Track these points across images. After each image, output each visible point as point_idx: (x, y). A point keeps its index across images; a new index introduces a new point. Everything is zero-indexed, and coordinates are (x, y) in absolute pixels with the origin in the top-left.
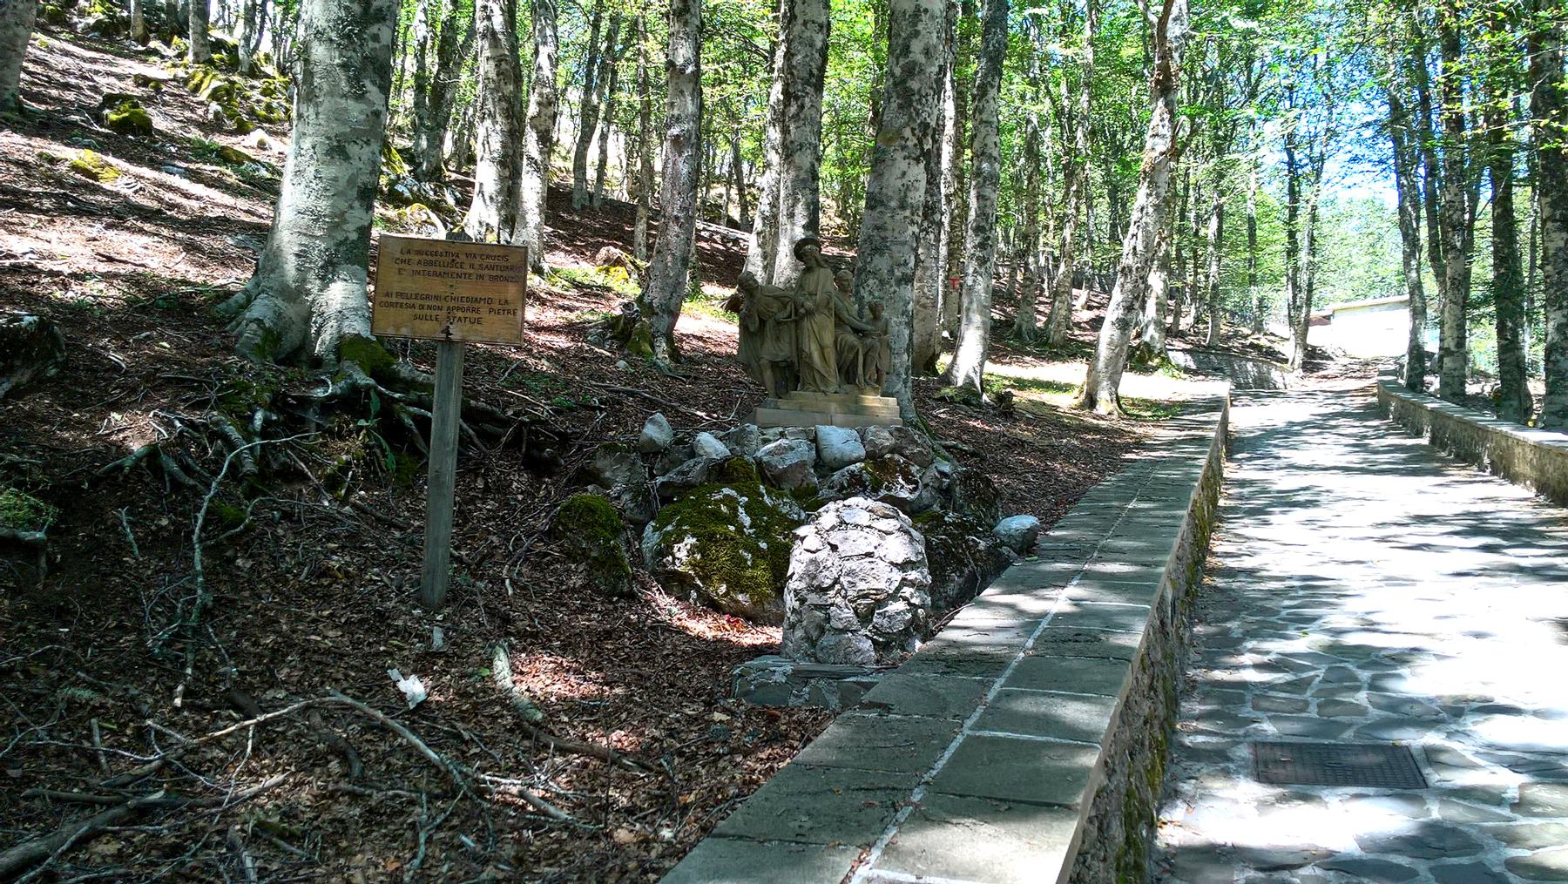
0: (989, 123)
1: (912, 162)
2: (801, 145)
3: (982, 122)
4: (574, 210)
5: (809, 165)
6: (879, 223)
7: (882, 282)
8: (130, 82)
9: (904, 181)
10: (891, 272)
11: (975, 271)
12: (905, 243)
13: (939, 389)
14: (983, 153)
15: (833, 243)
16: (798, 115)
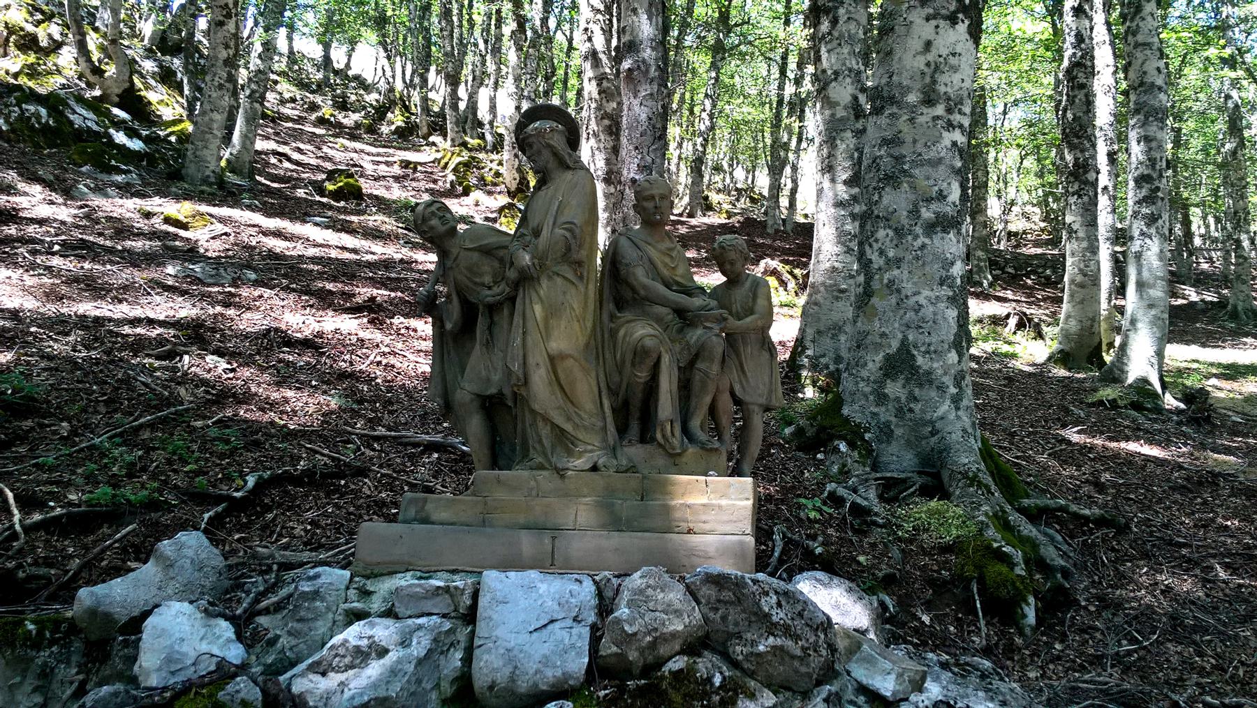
0: (1147, 45)
1: (942, 23)
2: (836, 73)
3: (1137, 45)
4: (768, 234)
5: (849, 98)
6: (888, 134)
7: (899, 233)
8: (396, 167)
9: (930, 57)
10: (914, 213)
11: (1142, 234)
12: (940, 161)
13: (1095, 390)
14: (1142, 84)
15: (1037, 244)
16: (830, 33)
